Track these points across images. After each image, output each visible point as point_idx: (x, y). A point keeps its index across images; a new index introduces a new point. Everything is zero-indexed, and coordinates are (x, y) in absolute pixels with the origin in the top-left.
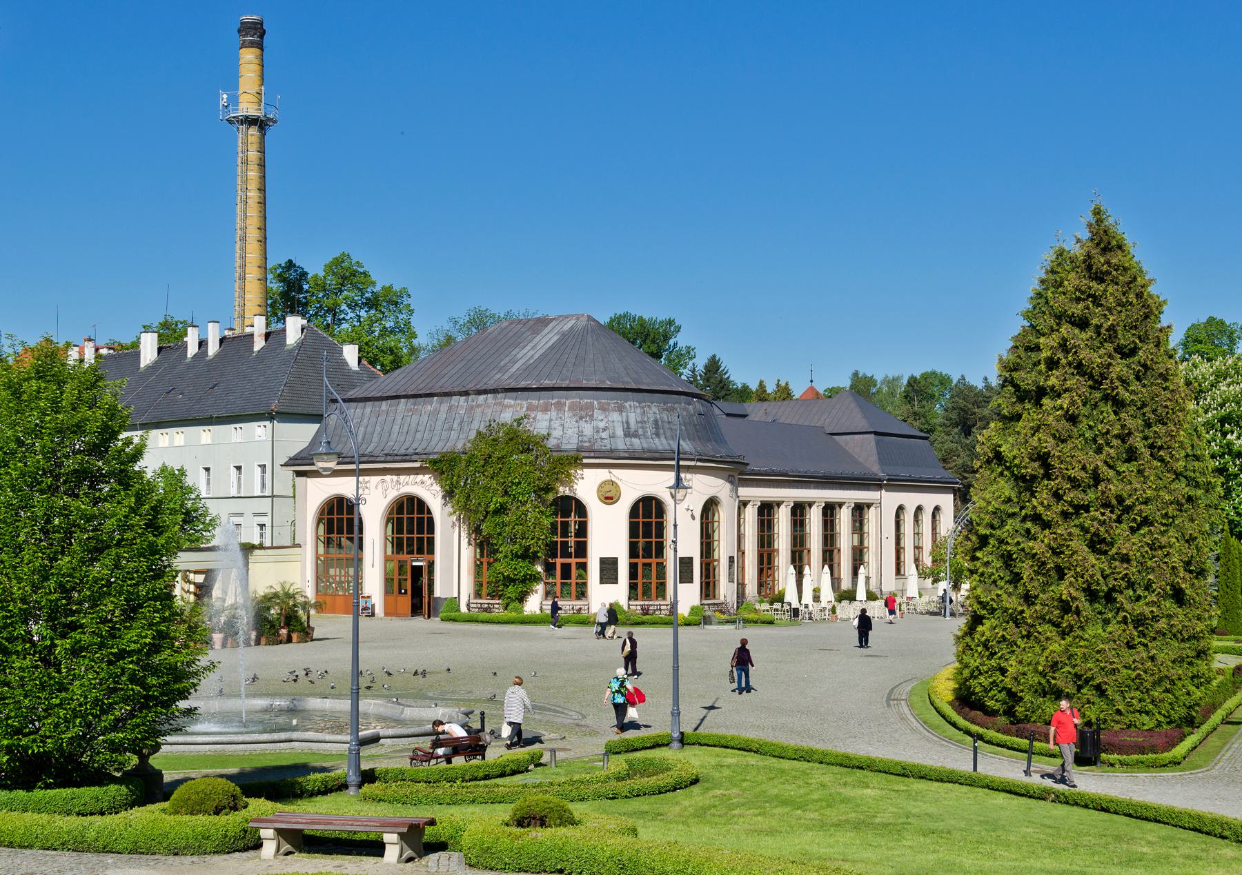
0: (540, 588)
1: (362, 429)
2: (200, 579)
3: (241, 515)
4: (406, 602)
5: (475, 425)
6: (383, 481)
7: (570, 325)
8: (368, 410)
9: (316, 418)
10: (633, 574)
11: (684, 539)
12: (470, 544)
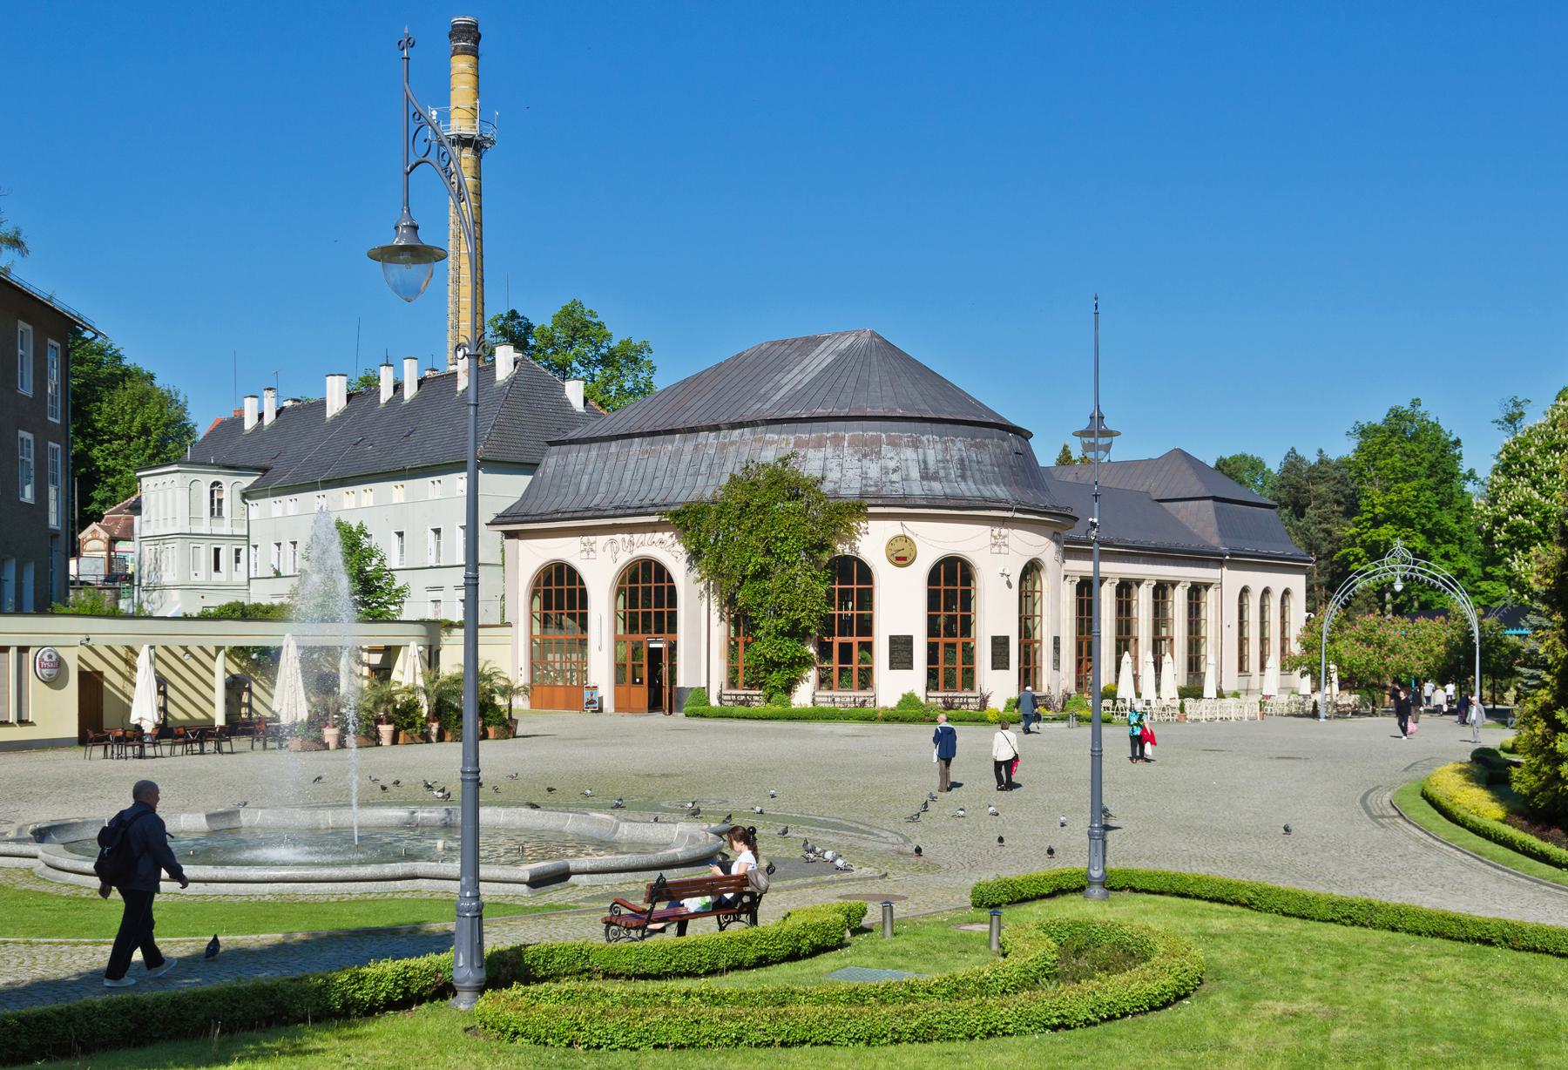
0: (812, 674)
1: (586, 477)
2: (376, 659)
3: (440, 588)
4: (642, 694)
5: (729, 468)
6: (612, 541)
7: (848, 343)
8: (594, 453)
9: (528, 467)
10: (932, 657)
11: (994, 613)
12: (722, 619)
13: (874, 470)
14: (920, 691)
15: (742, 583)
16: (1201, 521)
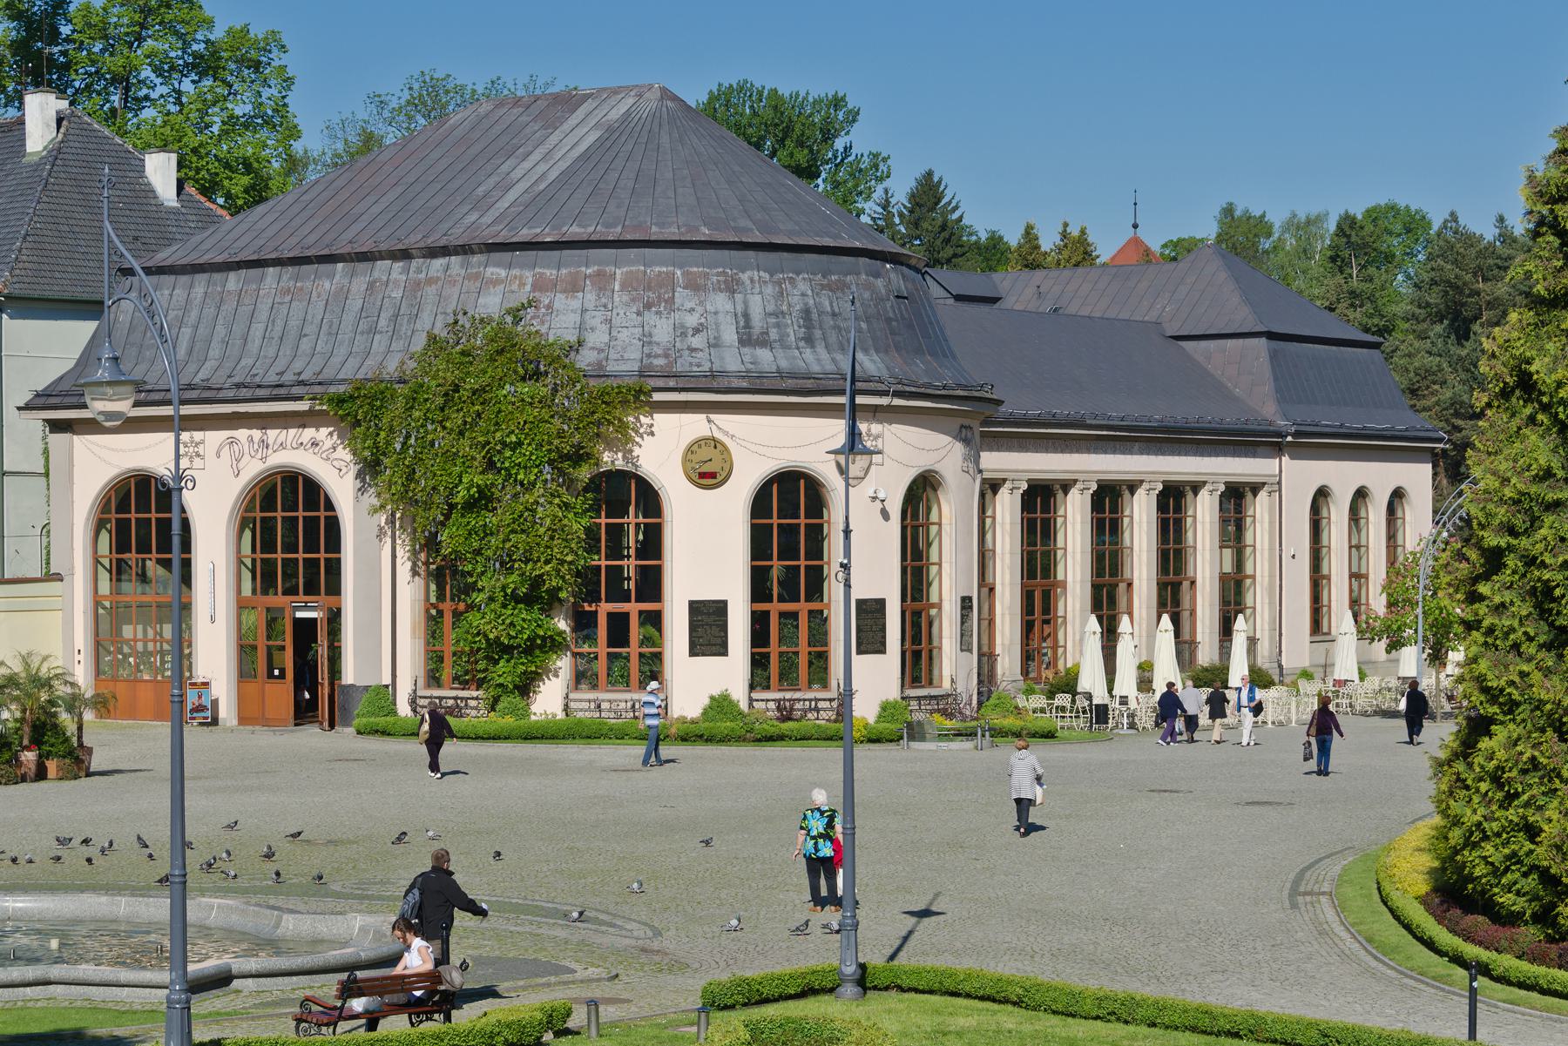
1: (186, 332)
4: (282, 694)
5: (425, 322)
6: (232, 442)
7: (623, 108)
8: (199, 291)
9: (89, 308)
11: (867, 562)
12: (415, 573)
13: (662, 330)
14: (739, 693)
15: (447, 516)
16: (1247, 378)
